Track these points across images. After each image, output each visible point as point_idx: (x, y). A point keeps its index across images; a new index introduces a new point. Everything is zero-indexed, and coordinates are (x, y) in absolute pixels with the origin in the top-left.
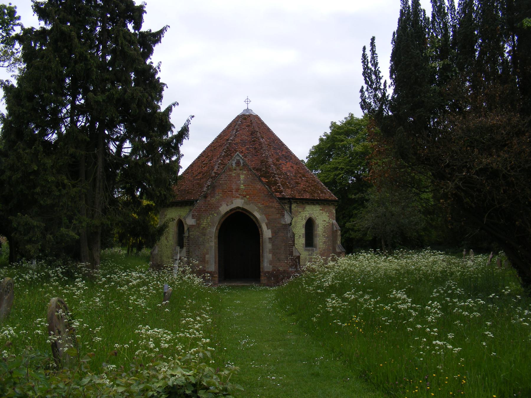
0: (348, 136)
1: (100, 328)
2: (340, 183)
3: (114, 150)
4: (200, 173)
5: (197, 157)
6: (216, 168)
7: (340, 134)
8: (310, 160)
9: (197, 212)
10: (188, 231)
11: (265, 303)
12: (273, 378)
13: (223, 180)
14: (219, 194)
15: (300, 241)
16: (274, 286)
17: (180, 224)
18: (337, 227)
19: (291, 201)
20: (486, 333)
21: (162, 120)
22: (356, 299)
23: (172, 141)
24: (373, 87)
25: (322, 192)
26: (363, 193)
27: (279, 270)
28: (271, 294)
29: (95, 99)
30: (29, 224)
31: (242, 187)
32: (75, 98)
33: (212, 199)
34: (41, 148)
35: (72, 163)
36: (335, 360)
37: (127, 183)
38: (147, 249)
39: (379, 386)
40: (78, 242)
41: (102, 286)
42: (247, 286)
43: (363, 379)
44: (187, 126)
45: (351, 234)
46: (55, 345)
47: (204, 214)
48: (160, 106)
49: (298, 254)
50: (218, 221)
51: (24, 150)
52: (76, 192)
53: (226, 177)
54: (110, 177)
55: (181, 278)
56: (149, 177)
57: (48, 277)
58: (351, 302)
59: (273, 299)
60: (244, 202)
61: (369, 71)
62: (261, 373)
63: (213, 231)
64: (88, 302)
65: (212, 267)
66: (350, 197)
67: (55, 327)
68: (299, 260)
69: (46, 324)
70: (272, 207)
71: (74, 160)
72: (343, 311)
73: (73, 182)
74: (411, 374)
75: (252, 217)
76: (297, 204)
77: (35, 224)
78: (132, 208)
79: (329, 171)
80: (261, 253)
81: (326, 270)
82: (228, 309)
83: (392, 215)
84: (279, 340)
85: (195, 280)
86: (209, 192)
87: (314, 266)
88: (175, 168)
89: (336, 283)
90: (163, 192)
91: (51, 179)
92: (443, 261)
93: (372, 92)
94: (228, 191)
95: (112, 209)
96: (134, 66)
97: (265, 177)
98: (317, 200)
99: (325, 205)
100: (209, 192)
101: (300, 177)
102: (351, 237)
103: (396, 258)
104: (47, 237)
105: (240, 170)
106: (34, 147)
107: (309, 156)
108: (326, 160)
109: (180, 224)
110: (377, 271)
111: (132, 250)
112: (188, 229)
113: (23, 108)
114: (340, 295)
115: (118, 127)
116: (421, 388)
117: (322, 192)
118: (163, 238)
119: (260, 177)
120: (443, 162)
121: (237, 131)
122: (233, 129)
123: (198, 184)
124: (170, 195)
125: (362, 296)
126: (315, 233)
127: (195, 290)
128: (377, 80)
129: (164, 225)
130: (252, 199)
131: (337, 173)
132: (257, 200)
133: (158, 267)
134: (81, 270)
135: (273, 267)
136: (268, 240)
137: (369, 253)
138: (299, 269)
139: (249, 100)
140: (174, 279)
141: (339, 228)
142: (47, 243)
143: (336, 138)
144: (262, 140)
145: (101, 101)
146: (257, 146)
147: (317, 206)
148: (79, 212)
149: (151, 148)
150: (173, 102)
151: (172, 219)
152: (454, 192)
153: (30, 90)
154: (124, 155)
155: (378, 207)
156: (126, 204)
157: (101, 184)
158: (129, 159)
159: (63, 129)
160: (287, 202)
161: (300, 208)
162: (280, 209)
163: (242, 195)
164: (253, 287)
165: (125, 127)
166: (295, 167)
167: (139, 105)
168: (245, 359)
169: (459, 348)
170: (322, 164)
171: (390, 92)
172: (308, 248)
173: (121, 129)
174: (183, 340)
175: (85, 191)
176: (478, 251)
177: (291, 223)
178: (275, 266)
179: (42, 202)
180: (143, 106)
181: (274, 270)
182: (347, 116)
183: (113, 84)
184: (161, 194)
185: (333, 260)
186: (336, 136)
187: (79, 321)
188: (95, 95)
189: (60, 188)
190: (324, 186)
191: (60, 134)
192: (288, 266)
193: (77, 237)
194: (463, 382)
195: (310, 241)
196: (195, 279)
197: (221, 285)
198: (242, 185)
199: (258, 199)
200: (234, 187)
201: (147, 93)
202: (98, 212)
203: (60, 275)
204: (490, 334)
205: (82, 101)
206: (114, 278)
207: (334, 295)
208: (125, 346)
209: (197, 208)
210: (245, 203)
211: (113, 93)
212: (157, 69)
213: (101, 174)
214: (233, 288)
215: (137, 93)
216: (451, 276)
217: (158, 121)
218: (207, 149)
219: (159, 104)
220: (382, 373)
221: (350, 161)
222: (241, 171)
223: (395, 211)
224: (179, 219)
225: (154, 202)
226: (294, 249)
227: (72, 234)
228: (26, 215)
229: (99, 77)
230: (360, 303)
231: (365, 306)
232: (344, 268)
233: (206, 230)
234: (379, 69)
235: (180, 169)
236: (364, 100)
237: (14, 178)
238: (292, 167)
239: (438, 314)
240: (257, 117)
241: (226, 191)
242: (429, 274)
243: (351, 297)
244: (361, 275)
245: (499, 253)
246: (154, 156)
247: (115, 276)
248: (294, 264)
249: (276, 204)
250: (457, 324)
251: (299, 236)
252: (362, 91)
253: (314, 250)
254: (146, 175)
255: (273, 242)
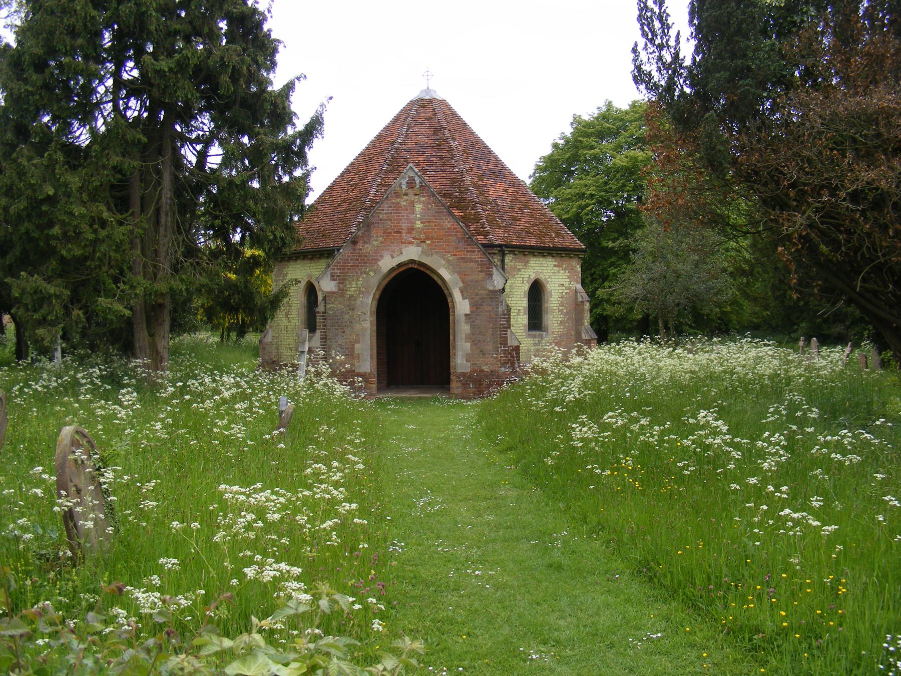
0: (602, 139)
1: (153, 484)
2: (589, 222)
3: (194, 160)
4: (344, 202)
5: (339, 174)
6: (373, 191)
7: (588, 136)
8: (534, 181)
9: (340, 269)
10: (323, 302)
11: (460, 429)
12: (477, 572)
13: (386, 213)
14: (377, 236)
15: (519, 320)
16: (475, 398)
17: (311, 290)
18: (583, 296)
19: (503, 249)
20: (886, 498)
21: (275, 105)
22: (624, 426)
23: (294, 142)
24: (657, 43)
25: (558, 235)
26: (627, 239)
27: (482, 371)
28: (469, 413)
29: (155, 67)
30: (41, 291)
31: (418, 224)
32: (120, 66)
33: (366, 246)
34: (60, 157)
35: (115, 182)
36: (590, 537)
37: (216, 217)
38: (254, 333)
39: (675, 592)
40: (129, 322)
41: (167, 401)
42: (427, 397)
43: (645, 576)
44: (321, 115)
45: (604, 309)
46: (69, 516)
47: (352, 273)
48: (272, 79)
49: (516, 344)
50: (377, 285)
51: (30, 159)
52: (124, 234)
53: (391, 207)
54: (185, 207)
55: (312, 383)
56: (254, 207)
57: (76, 383)
58: (615, 431)
59: (472, 422)
60: (422, 252)
61: (649, 14)
62: (455, 563)
63: (367, 303)
64: (142, 430)
65: (367, 364)
66: (606, 245)
67: (69, 482)
68: (518, 353)
69: (52, 478)
70: (471, 261)
71: (120, 176)
72: (602, 446)
73: (119, 217)
74: (738, 571)
75: (435, 278)
76: (515, 254)
77: (52, 291)
78: (224, 261)
79: (569, 199)
80: (451, 342)
81: (568, 372)
82: (394, 440)
83: (678, 277)
84: (486, 499)
85: (336, 389)
86: (360, 233)
87: (545, 365)
88: (300, 190)
89: (585, 395)
90: (279, 234)
91: (78, 210)
92: (773, 357)
93: (654, 52)
94: (394, 232)
95: (188, 264)
96: (225, 6)
97: (458, 208)
98: (549, 249)
99: (562, 257)
100: (360, 233)
101: (520, 209)
102: (605, 313)
103: (690, 352)
104: (74, 313)
105: (415, 195)
106: (48, 153)
107: (534, 173)
108: (564, 182)
109: (311, 290)
110: (658, 374)
111: (229, 336)
112: (324, 299)
113: (26, 85)
114: (596, 417)
115: (200, 119)
116: (759, 597)
117: (558, 235)
118: (280, 315)
119: (449, 207)
120: (785, 178)
121: (409, 127)
122: (403, 125)
123: (341, 220)
124: (292, 238)
125: (637, 420)
126: (546, 305)
127: (336, 406)
128: (663, 31)
129: (281, 291)
130: (436, 246)
131: (584, 203)
132: (443, 249)
133: (272, 365)
134: (135, 372)
135: (472, 364)
136: (463, 318)
137: (642, 342)
138: (518, 369)
139: (429, 74)
140: (299, 387)
141: (586, 298)
142: (74, 324)
143: (581, 142)
144: (454, 144)
145: (166, 69)
146: (444, 153)
147: (550, 259)
148: (130, 269)
149: (257, 155)
150: (298, 75)
151: (296, 280)
152: (804, 233)
153: (39, 51)
154: (209, 168)
155: (653, 262)
156: (215, 255)
157: (169, 219)
158: (218, 174)
159: (100, 121)
160: (497, 252)
161: (519, 262)
162: (485, 265)
163: (417, 239)
164: (437, 399)
165: (213, 119)
166: (510, 190)
167: (235, 78)
168: (425, 534)
169: (833, 527)
170: (556, 188)
171: (688, 51)
172: (534, 333)
173: (205, 123)
174: (311, 504)
175: (141, 231)
176: (827, 340)
177: (503, 289)
178: (476, 364)
179: (64, 252)
180: (242, 79)
181: (475, 371)
182: (602, 104)
183: (187, 40)
184: (275, 235)
185: (579, 354)
186: (581, 139)
187: (114, 471)
188: (156, 60)
189: (96, 226)
190: (562, 225)
191: (93, 132)
192: (499, 363)
193: (127, 313)
194: (840, 590)
195: (536, 321)
196: (336, 387)
197: (381, 396)
198: (419, 222)
199: (446, 245)
200: (405, 225)
201: (249, 56)
202: (164, 269)
203: (98, 382)
204: (892, 500)
205: (136, 73)
206: (192, 386)
207: (584, 417)
208: (192, 525)
209: (340, 263)
210: (424, 252)
211: (187, 55)
212: (266, 13)
213: (169, 201)
214: (403, 401)
215: (231, 55)
216: (788, 384)
217: (268, 107)
218: (357, 158)
219: (271, 76)
220: (682, 567)
221: (606, 183)
222: (417, 197)
223: (683, 270)
224: (309, 281)
225: (264, 250)
226: (509, 333)
227: (119, 307)
228: (36, 276)
229: (161, 27)
230: (632, 432)
231: (642, 438)
232: (599, 368)
233: (355, 300)
234: (667, 11)
235: (311, 193)
236: (638, 68)
237: (12, 210)
238: (506, 191)
239: (781, 456)
240: (444, 103)
241: (390, 233)
242: (750, 379)
243: (616, 422)
244: (628, 380)
245: (863, 344)
246: (262, 169)
247: (194, 381)
248: (509, 360)
249: (477, 256)
250: (816, 474)
251: (517, 311)
252: (634, 50)
253: (544, 336)
254: (247, 202)
255: (473, 322)
